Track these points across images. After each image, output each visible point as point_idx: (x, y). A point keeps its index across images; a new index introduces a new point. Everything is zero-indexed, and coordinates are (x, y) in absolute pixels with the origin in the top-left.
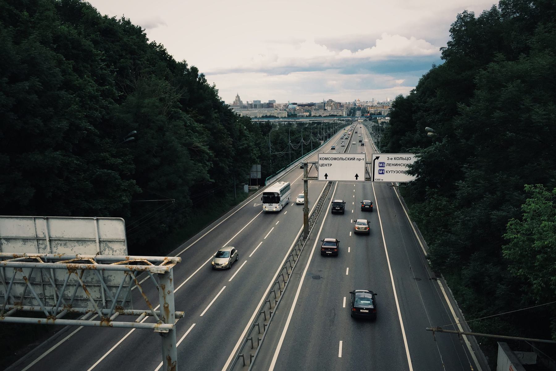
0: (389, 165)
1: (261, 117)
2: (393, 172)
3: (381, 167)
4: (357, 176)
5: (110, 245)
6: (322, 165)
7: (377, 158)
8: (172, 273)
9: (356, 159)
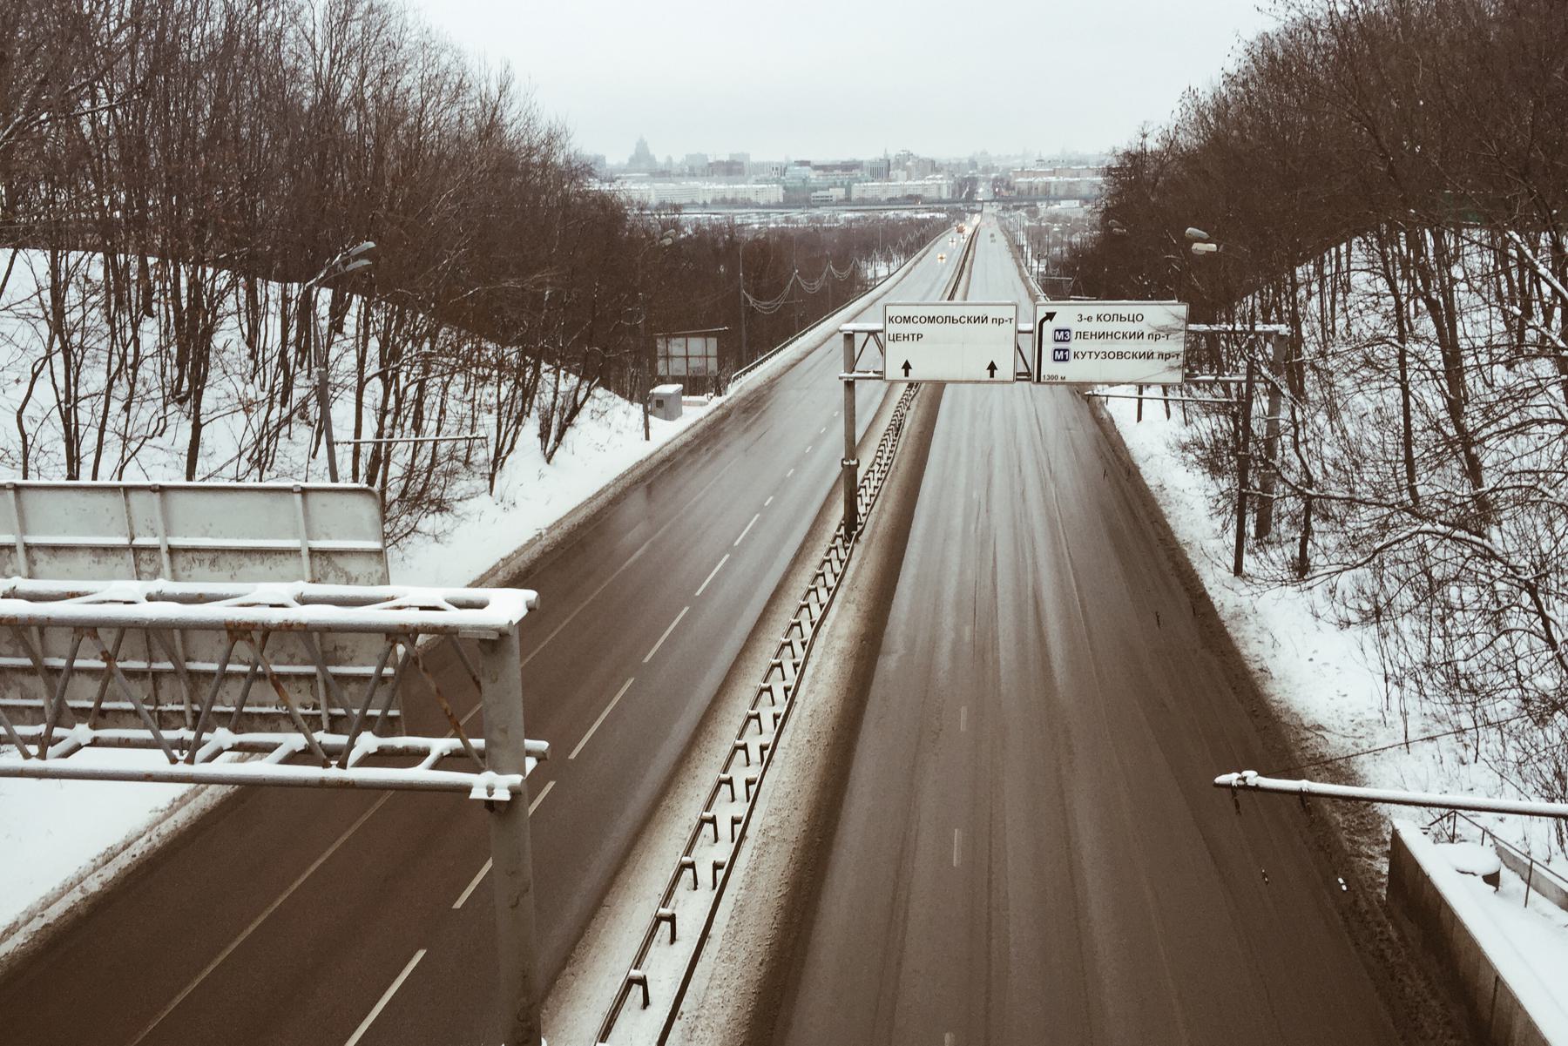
0: (1083, 335)
1: (709, 201)
2: (1093, 355)
3: (1061, 341)
4: (992, 367)
5: (340, 562)
6: (896, 338)
7: (1050, 316)
8: (515, 642)
9: (990, 320)
